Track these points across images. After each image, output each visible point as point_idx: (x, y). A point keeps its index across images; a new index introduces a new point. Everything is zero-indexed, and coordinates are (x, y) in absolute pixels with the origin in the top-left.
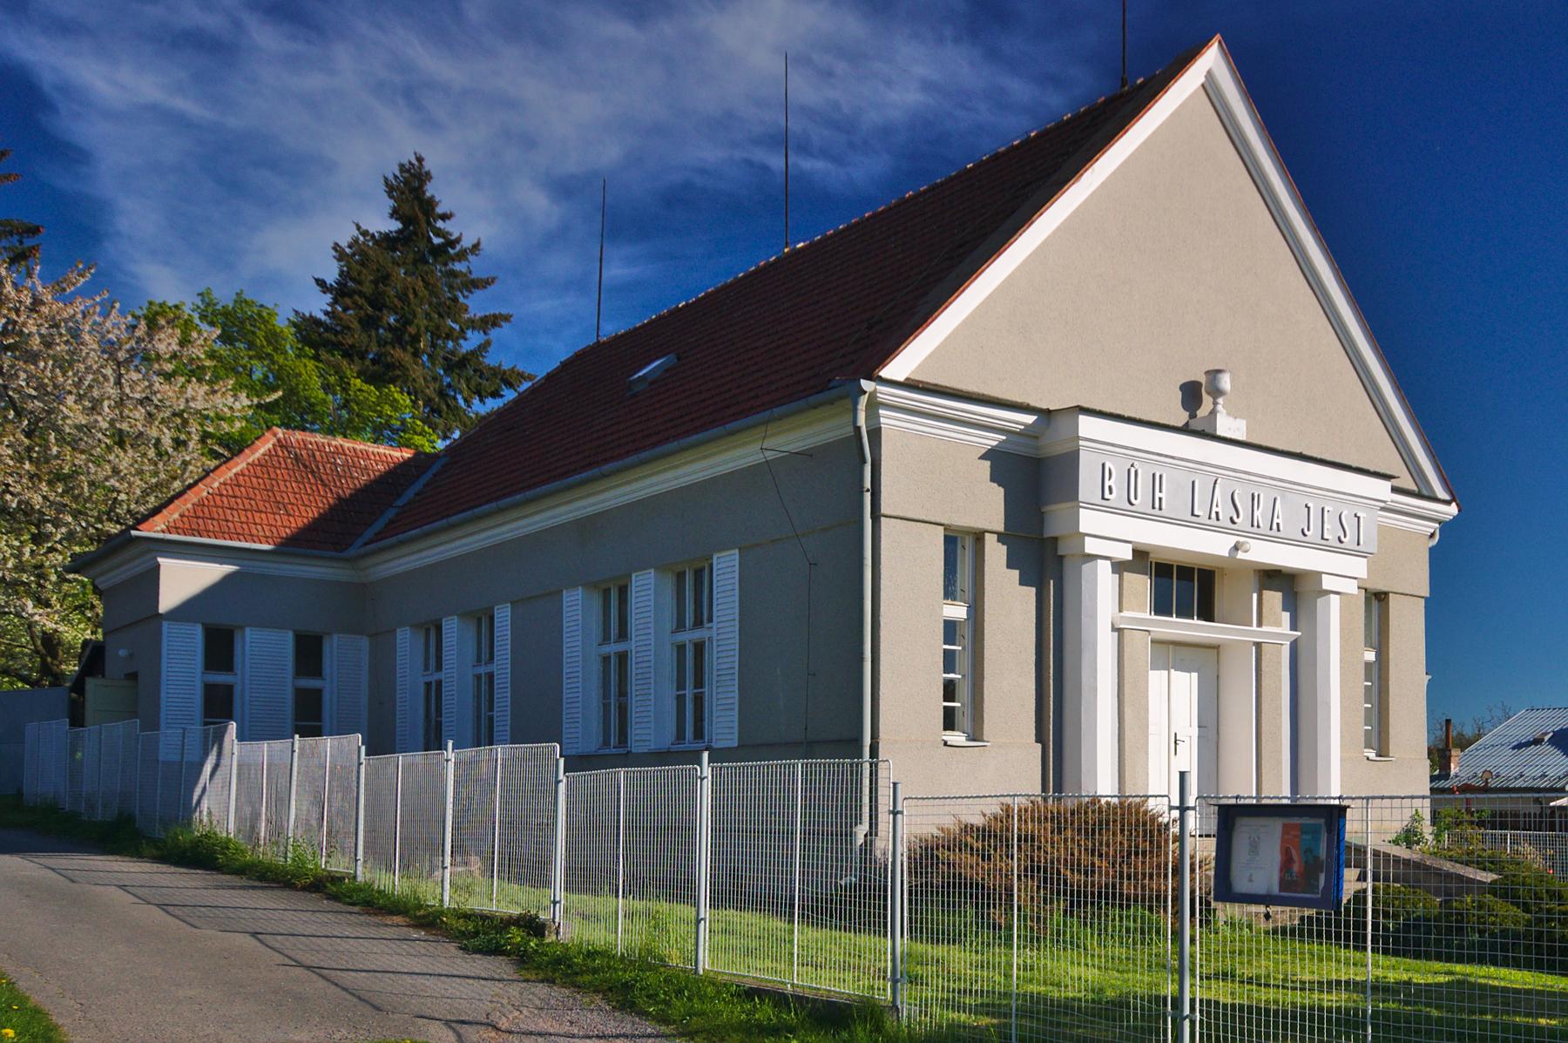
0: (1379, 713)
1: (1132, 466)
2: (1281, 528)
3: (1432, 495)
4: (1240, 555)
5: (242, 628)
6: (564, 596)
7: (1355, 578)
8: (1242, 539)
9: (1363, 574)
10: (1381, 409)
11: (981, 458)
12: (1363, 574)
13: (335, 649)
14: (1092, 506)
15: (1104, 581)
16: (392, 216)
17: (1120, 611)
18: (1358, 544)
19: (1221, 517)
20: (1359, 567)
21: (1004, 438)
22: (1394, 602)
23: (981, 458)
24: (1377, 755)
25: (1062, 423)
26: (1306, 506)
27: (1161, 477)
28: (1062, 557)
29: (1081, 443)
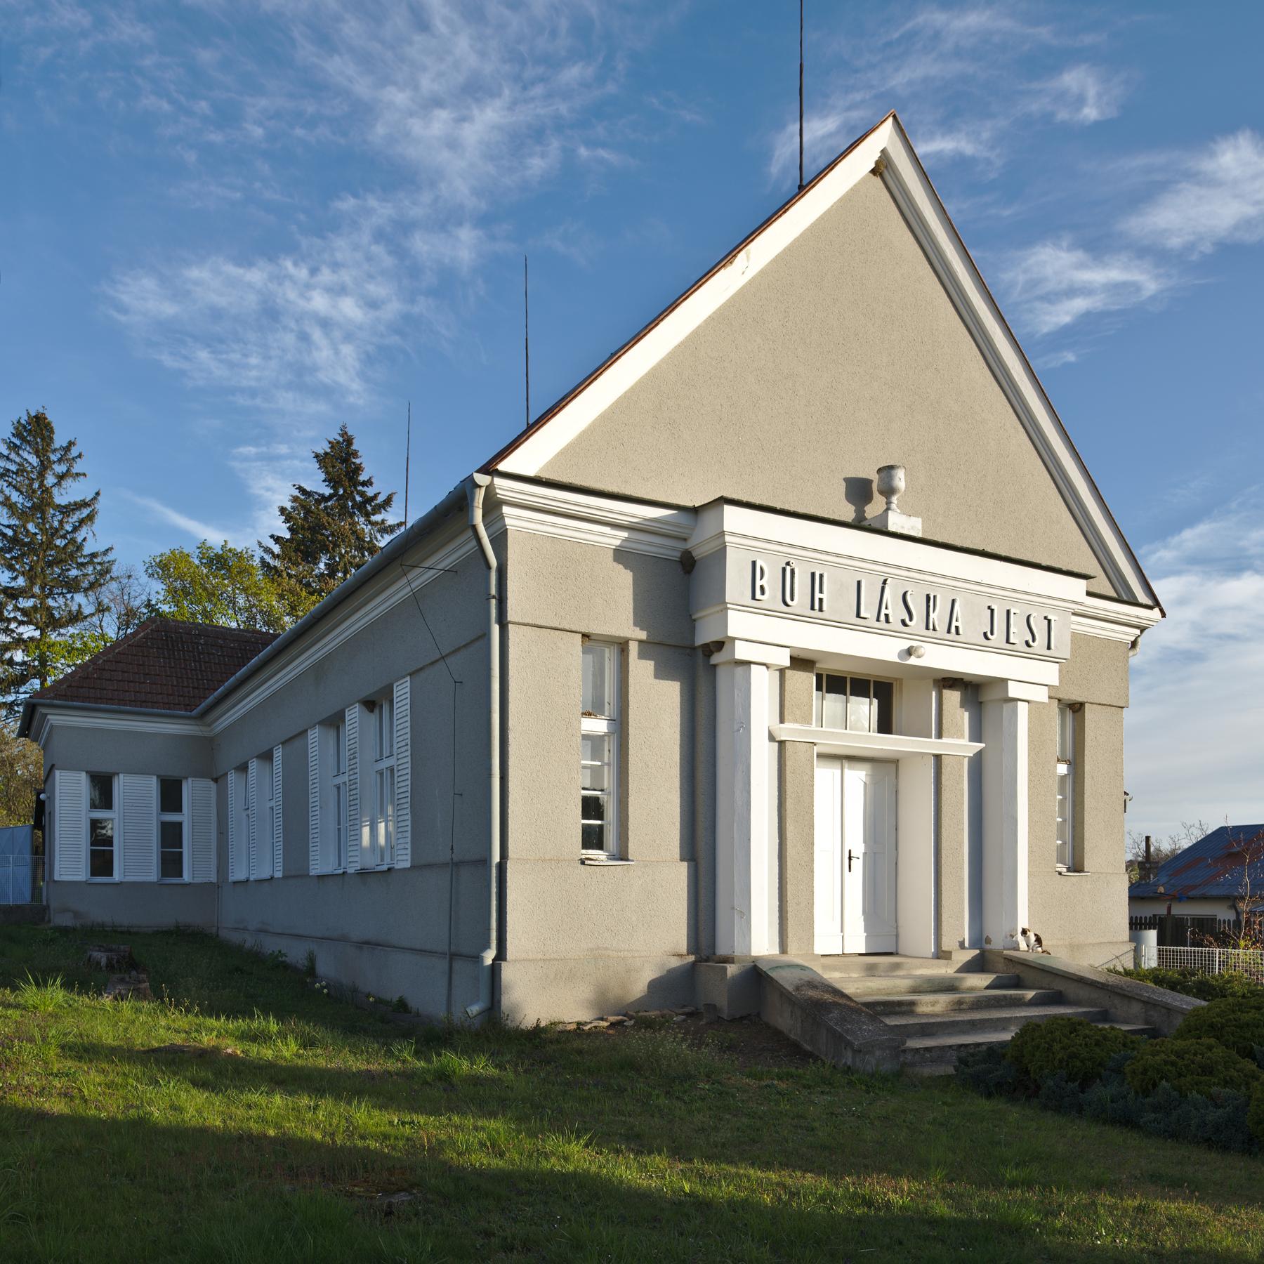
0: (1073, 827)
1: (788, 564)
2: (961, 632)
3: (1132, 600)
4: (913, 661)
5: (118, 774)
6: (309, 734)
7: (1046, 685)
8: (914, 644)
9: (1055, 681)
12: (1055, 681)
13: (188, 790)
14: (743, 608)
15: (762, 687)
16: (322, 459)
17: (782, 721)
18: (1049, 648)
19: (891, 619)
20: (1050, 673)
22: (1089, 712)
25: (707, 522)
26: (989, 608)
27: (821, 576)
29: (727, 538)
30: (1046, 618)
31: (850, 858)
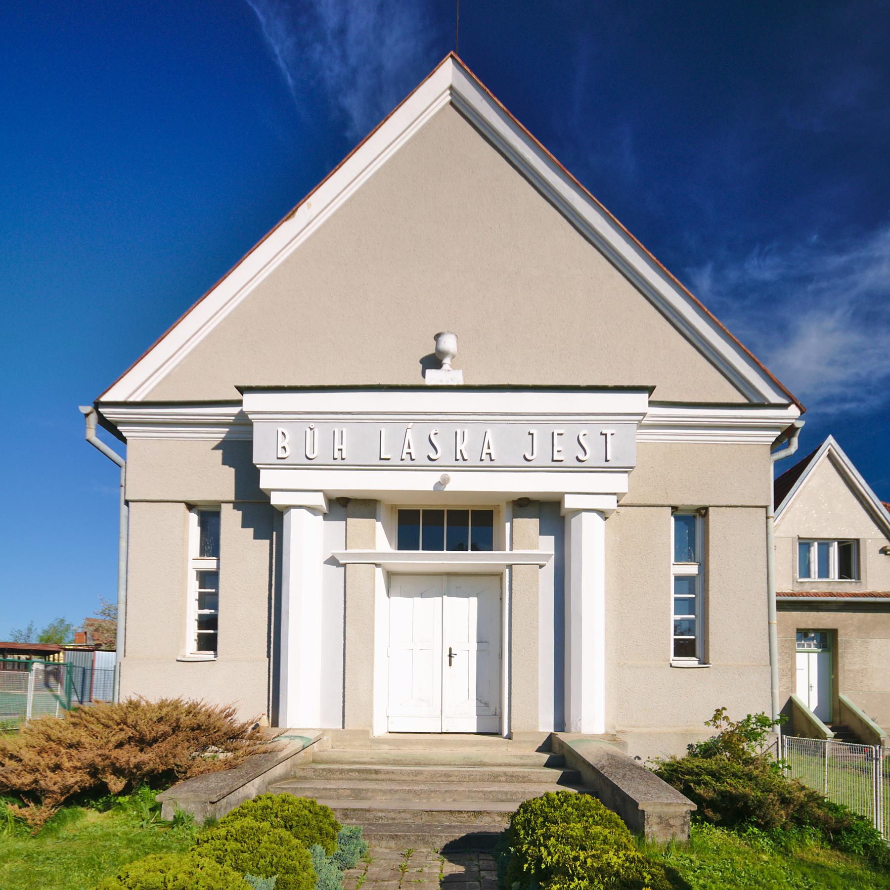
7: (615, 494)
10: (687, 333)
11: (214, 449)
21: (227, 430)
23: (214, 449)
24: (699, 664)
28: (563, 517)
30: (602, 434)
31: (450, 656)
